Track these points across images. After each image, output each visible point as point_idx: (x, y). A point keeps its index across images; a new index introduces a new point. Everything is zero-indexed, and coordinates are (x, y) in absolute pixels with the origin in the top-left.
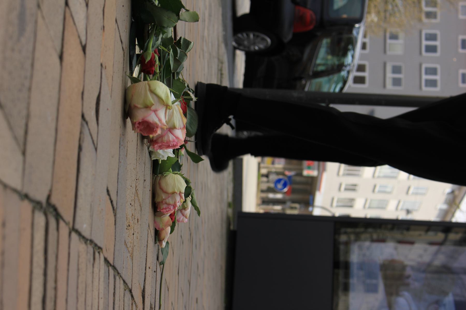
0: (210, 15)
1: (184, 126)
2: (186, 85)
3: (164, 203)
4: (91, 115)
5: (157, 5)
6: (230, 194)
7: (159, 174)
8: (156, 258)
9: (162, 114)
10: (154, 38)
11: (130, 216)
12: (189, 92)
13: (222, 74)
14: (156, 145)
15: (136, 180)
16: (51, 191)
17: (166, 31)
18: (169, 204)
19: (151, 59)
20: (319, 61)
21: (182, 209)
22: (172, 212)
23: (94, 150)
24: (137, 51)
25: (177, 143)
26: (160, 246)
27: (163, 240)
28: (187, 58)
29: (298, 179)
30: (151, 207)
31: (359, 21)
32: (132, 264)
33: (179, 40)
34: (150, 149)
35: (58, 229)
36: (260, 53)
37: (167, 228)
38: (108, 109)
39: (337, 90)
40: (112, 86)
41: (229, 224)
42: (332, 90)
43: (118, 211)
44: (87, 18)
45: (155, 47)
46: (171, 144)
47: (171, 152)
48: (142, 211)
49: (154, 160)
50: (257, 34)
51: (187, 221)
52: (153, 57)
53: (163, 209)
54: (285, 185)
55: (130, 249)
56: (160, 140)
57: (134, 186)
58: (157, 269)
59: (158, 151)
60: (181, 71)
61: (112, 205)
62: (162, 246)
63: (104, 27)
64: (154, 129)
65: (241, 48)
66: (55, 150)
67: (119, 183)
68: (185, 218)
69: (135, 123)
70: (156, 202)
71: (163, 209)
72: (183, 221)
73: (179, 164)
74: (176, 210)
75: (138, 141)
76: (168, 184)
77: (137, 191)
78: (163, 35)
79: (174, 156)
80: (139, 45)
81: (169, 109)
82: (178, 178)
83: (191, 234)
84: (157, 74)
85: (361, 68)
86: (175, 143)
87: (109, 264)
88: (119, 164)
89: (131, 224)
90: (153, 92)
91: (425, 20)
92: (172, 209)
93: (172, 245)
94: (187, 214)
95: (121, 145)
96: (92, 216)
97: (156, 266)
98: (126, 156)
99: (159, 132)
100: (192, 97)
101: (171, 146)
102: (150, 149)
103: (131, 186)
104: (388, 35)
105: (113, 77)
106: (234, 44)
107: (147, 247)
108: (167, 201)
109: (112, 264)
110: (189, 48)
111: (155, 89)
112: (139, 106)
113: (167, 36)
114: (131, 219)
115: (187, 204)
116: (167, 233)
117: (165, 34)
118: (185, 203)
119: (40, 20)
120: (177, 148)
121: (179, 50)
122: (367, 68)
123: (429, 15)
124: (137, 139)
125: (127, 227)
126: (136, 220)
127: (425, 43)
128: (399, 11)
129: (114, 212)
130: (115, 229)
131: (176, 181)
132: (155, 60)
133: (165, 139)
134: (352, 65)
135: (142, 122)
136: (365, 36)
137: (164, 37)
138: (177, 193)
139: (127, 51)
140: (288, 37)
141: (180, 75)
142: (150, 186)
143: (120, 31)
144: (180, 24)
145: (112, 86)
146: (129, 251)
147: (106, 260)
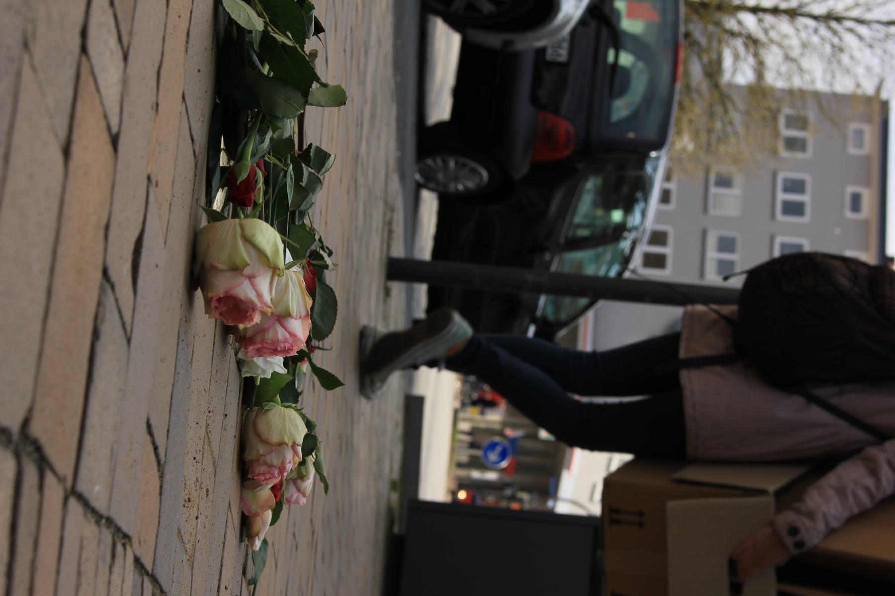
0: (373, 117)
1: (308, 312)
2: (317, 237)
3: (261, 462)
4: (121, 272)
5: (266, 72)
6: (397, 466)
7: (255, 405)
8: (241, 571)
9: (264, 283)
10: (257, 137)
11: (191, 482)
12: (322, 252)
13: (390, 232)
14: (251, 348)
15: (207, 412)
16: (30, 410)
17: (280, 126)
18: (271, 466)
19: (249, 175)
20: (577, 220)
21: (297, 479)
22: (276, 481)
23: (124, 341)
24: (223, 161)
25: (291, 344)
26: (249, 546)
27: (257, 535)
28: (322, 187)
29: (529, 444)
30: (235, 469)
31: (659, 145)
32: (191, 576)
33: (306, 149)
34: (240, 355)
35: (41, 487)
36: (467, 197)
37: (265, 512)
38: (157, 266)
39: (613, 273)
40: (168, 222)
41: (391, 523)
42: (602, 272)
43: (168, 469)
44: (125, 81)
45: (257, 157)
46: (280, 347)
47: (279, 364)
48: (216, 476)
49: (247, 377)
50: (462, 160)
51: (305, 502)
52: (253, 174)
53: (259, 474)
54: (503, 455)
55: (189, 546)
56: (258, 338)
57: (203, 423)
58: (241, 591)
59: (255, 359)
60: (308, 209)
61: (157, 455)
62: (254, 547)
63: (157, 105)
64: (247, 312)
65: (432, 185)
66: (44, 331)
67: (172, 414)
68: (301, 496)
69: (211, 298)
70: (246, 461)
71: (259, 474)
72: (297, 502)
73: (296, 390)
74: (284, 478)
75: (217, 337)
76: (271, 427)
77: (210, 434)
78: (274, 133)
79: (285, 371)
80: (226, 150)
81: (279, 276)
82: (290, 414)
83: (313, 533)
84: (259, 207)
85: (658, 238)
86: (288, 344)
87: (144, 571)
88: (174, 376)
89: (194, 496)
90: (249, 241)
91: (784, 153)
92: (276, 475)
93: (274, 550)
94: (306, 488)
95: (181, 339)
96: (113, 471)
97: (240, 587)
98: (191, 363)
99: (257, 319)
100: (327, 263)
101: (279, 349)
102: (240, 355)
103: (197, 423)
104: (712, 178)
105: (172, 204)
106: (418, 177)
107: (224, 547)
108: (268, 459)
109: (150, 572)
110: (326, 165)
111: (254, 235)
112: (220, 266)
113: (282, 135)
114: (194, 488)
115: (306, 468)
116: (264, 523)
117: (279, 130)
118: (303, 468)
119: (27, 72)
120: (293, 355)
121: (306, 170)
122: (671, 239)
123: (792, 144)
124: (215, 333)
125: (184, 503)
126: (204, 490)
127: (782, 196)
128: (736, 133)
129: (159, 470)
130: (160, 503)
131: (287, 420)
132: (256, 179)
133: (270, 335)
134: (641, 229)
135: (223, 297)
136: (668, 178)
137: (275, 136)
138: (288, 445)
139: (202, 159)
140: (521, 169)
141: (307, 217)
142: (235, 429)
143: (190, 119)
144: (311, 112)
145: (168, 222)
146: (186, 551)
147: (137, 561)
